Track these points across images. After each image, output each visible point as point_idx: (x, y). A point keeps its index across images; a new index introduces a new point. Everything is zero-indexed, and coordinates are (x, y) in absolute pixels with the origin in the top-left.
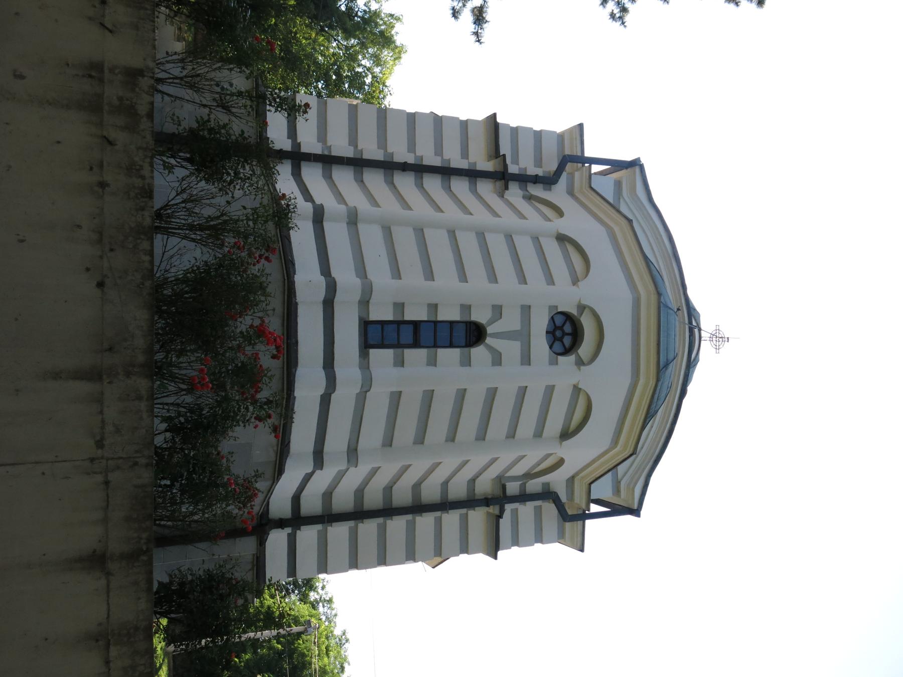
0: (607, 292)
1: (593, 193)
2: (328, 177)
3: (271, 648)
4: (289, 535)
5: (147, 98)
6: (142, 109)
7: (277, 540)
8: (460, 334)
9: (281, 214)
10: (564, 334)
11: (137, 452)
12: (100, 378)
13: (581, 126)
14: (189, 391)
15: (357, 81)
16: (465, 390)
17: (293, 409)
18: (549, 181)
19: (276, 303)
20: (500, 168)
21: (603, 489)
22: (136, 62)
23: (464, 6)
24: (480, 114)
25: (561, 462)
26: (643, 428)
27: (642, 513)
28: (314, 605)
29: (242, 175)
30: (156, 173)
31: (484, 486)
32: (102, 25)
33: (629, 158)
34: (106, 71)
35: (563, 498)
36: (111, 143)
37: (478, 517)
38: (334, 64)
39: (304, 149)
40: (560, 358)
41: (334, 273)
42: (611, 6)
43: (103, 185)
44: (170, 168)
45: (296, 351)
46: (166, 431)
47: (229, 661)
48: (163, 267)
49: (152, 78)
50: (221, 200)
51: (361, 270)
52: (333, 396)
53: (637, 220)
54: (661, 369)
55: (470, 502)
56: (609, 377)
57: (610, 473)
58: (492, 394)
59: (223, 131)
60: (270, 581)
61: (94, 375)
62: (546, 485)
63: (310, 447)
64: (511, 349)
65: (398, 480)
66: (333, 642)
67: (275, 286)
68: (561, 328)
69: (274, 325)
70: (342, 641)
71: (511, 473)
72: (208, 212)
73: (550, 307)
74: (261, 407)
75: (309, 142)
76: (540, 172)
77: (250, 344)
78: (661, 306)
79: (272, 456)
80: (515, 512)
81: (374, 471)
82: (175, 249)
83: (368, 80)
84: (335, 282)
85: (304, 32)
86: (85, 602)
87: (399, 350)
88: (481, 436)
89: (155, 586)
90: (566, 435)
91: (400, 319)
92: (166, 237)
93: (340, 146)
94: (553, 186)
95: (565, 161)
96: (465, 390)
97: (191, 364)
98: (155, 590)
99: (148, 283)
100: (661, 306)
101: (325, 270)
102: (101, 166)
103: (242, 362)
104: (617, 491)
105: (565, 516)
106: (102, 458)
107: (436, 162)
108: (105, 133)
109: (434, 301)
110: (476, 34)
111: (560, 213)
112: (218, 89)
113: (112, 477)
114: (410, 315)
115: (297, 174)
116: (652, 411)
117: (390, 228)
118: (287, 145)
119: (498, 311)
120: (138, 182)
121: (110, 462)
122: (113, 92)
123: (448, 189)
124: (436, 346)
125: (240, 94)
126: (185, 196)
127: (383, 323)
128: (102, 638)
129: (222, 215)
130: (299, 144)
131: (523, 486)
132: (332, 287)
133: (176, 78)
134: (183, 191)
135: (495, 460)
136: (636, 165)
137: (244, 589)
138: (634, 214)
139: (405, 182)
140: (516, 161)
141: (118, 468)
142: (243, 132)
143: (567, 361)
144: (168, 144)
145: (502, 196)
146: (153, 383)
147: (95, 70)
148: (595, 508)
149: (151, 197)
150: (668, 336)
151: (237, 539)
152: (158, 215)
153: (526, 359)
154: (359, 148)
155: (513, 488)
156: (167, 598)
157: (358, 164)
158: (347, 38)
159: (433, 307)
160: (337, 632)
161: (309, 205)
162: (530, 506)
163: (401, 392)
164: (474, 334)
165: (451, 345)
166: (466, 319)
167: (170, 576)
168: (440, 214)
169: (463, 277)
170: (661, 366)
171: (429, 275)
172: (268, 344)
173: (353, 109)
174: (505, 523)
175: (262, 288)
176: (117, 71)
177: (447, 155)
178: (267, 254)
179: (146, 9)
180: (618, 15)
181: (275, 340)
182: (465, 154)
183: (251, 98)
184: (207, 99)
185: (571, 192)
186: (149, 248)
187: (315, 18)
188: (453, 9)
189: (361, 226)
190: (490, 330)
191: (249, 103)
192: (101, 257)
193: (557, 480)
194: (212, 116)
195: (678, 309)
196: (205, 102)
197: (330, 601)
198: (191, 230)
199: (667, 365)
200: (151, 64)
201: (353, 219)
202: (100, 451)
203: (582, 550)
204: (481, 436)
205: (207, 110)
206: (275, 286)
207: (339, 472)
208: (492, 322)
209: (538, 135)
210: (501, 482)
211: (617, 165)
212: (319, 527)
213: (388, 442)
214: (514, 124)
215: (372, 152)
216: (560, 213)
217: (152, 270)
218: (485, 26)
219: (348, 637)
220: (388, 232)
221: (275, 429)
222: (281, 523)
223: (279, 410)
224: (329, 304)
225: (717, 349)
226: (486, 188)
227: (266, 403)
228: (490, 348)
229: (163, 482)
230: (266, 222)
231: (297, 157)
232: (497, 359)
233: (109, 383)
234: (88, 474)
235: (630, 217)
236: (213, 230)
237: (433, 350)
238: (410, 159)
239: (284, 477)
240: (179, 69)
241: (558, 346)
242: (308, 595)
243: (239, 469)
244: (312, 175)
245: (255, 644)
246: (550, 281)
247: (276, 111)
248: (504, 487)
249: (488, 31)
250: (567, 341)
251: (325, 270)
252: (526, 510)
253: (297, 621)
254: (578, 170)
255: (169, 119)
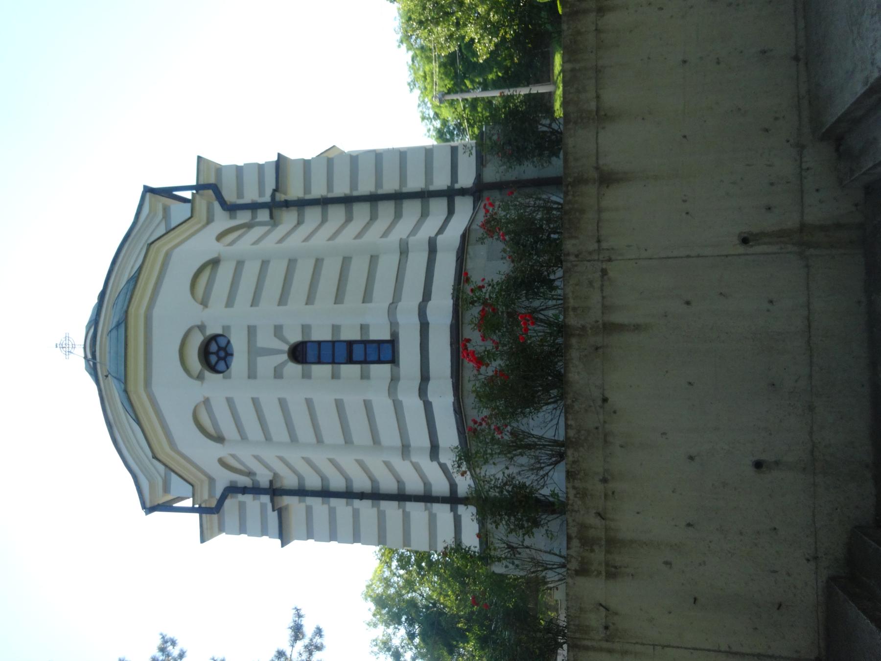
0: (176, 390)
1: (191, 481)
2: (427, 484)
3: (472, 82)
4: (457, 182)
5: (572, 552)
6: (575, 543)
7: (466, 179)
8: (311, 353)
9: (467, 456)
10: (217, 353)
11: (576, 266)
12: (604, 324)
13: (203, 540)
14: (536, 310)
15: (404, 563)
16: (307, 304)
17: (454, 290)
18: (232, 490)
19: (468, 386)
20: (278, 499)
21: (179, 212)
22: (581, 581)
23: (311, 640)
24: (296, 545)
25: (219, 237)
26: (140, 268)
27: (142, 189)
28: (437, 115)
29: (497, 490)
30: (564, 490)
31: (289, 218)
32: (607, 609)
33: (156, 514)
34: (604, 573)
35: (217, 205)
36: (599, 514)
37: (295, 191)
38: (424, 576)
39: (447, 507)
40: (220, 332)
41: (420, 404)
42: (175, 652)
43: (604, 481)
44: (554, 494)
45: (451, 337)
46: (554, 280)
47: (506, 73)
48: (558, 412)
49: (568, 569)
50: (513, 470)
51: (398, 406)
52: (421, 299)
53: (147, 457)
54: (123, 322)
55: (302, 204)
56: (174, 316)
57: (173, 225)
58: (283, 300)
59: (512, 527)
60: (471, 153)
61: (610, 328)
62: (232, 217)
63: (440, 256)
64: (265, 340)
65: (365, 227)
66: (420, 84)
67: (470, 400)
68: (220, 359)
69: (469, 367)
70: (412, 84)
71: (266, 228)
72: (523, 460)
73: (229, 377)
74: (479, 299)
75: (443, 512)
76: (241, 497)
77: (488, 351)
78: (124, 380)
79: (471, 250)
80: (261, 193)
81: (385, 234)
82: (549, 426)
83: (395, 564)
84: (420, 396)
85: (449, 603)
86: (616, 145)
87: (365, 338)
88: (292, 263)
89: (561, 155)
90: (215, 263)
91: (364, 366)
92: (556, 438)
93: (417, 510)
94: (228, 485)
95: (217, 509)
96: (307, 304)
97: (536, 333)
98: (562, 152)
99: (569, 402)
100: (124, 380)
101: (428, 407)
102: (606, 495)
103: (495, 333)
104: (166, 210)
105: (215, 189)
106: (602, 261)
107: (334, 501)
108: (603, 522)
109: (335, 381)
110: (300, 616)
111: (222, 462)
112: (516, 562)
113: (596, 246)
114: (355, 369)
115: (453, 486)
116: (132, 283)
117: (374, 443)
118: (461, 509)
119: (278, 373)
120: (577, 483)
121: (596, 258)
122: (598, 556)
123: (323, 478)
124: (333, 343)
125: (499, 560)
126: (542, 473)
127: (379, 361)
128: (602, 117)
129: (512, 458)
130: (452, 510)
131: (254, 217)
132: (423, 392)
133: (551, 569)
134: (543, 477)
135: (280, 241)
136: (149, 509)
137: (492, 148)
138: (152, 464)
139: (361, 483)
140: (263, 506)
141: (590, 253)
142: (497, 528)
143: (213, 329)
144: (553, 507)
145: (276, 475)
146: (564, 320)
147: (612, 573)
148: (188, 194)
149: (568, 472)
150: (117, 353)
151: (498, 180)
152: (562, 456)
153: (252, 331)
154: (401, 510)
155: (263, 215)
156: (552, 144)
157: (401, 497)
158: (412, 598)
159: (335, 376)
160: (417, 92)
161: (442, 460)
162: (248, 199)
163: (363, 302)
164: (299, 353)
165: (319, 343)
166: (306, 366)
167: (550, 162)
168: (331, 457)
169: (309, 403)
170: (123, 325)
171: (339, 405)
172: (474, 352)
173: (406, 542)
174: (270, 185)
175: (478, 396)
176: (595, 573)
177: (325, 508)
178: (476, 426)
179: (574, 625)
180: (169, 644)
181: (468, 355)
182: (309, 510)
183: (491, 557)
184: (525, 553)
185: (212, 481)
186: (569, 431)
187: (441, 613)
188: (321, 636)
189: (398, 443)
190: (285, 357)
191: (492, 553)
192: (605, 422)
193: (222, 221)
194: (521, 539)
195: (107, 376)
196: (528, 550)
197: (423, 118)
198: (537, 445)
199: (118, 325)
200: (570, 581)
201: (406, 450)
202: (604, 266)
203: (199, 158)
204: (292, 263)
205: (526, 543)
206: (470, 400)
207: (414, 235)
208: (283, 364)
209: (242, 529)
210: (274, 221)
211: (167, 507)
212: (432, 188)
213: (374, 260)
214: (265, 538)
215: (391, 508)
216: (222, 462)
217: (566, 412)
218: (292, 624)
219: (408, 87)
220: (376, 440)
221: (467, 280)
222: (463, 192)
223: (465, 296)
224: (425, 378)
225: (67, 337)
226: (290, 481)
227: (476, 301)
228: (284, 340)
229: (556, 236)
230: (477, 453)
231: (453, 500)
232: (278, 331)
233: (597, 322)
234: (613, 249)
235: (155, 461)
236: (521, 444)
237: (335, 339)
238: (357, 503)
239: (461, 232)
240: (548, 576)
241: (222, 342)
242: (442, 125)
243: (498, 245)
244: (440, 486)
245: (485, 87)
246: (230, 402)
247: (469, 548)
248: (271, 217)
249: (289, 620)
250: (213, 347)
251: (428, 407)
252: (251, 195)
253: (452, 103)
254: (205, 501)
255: (555, 534)
